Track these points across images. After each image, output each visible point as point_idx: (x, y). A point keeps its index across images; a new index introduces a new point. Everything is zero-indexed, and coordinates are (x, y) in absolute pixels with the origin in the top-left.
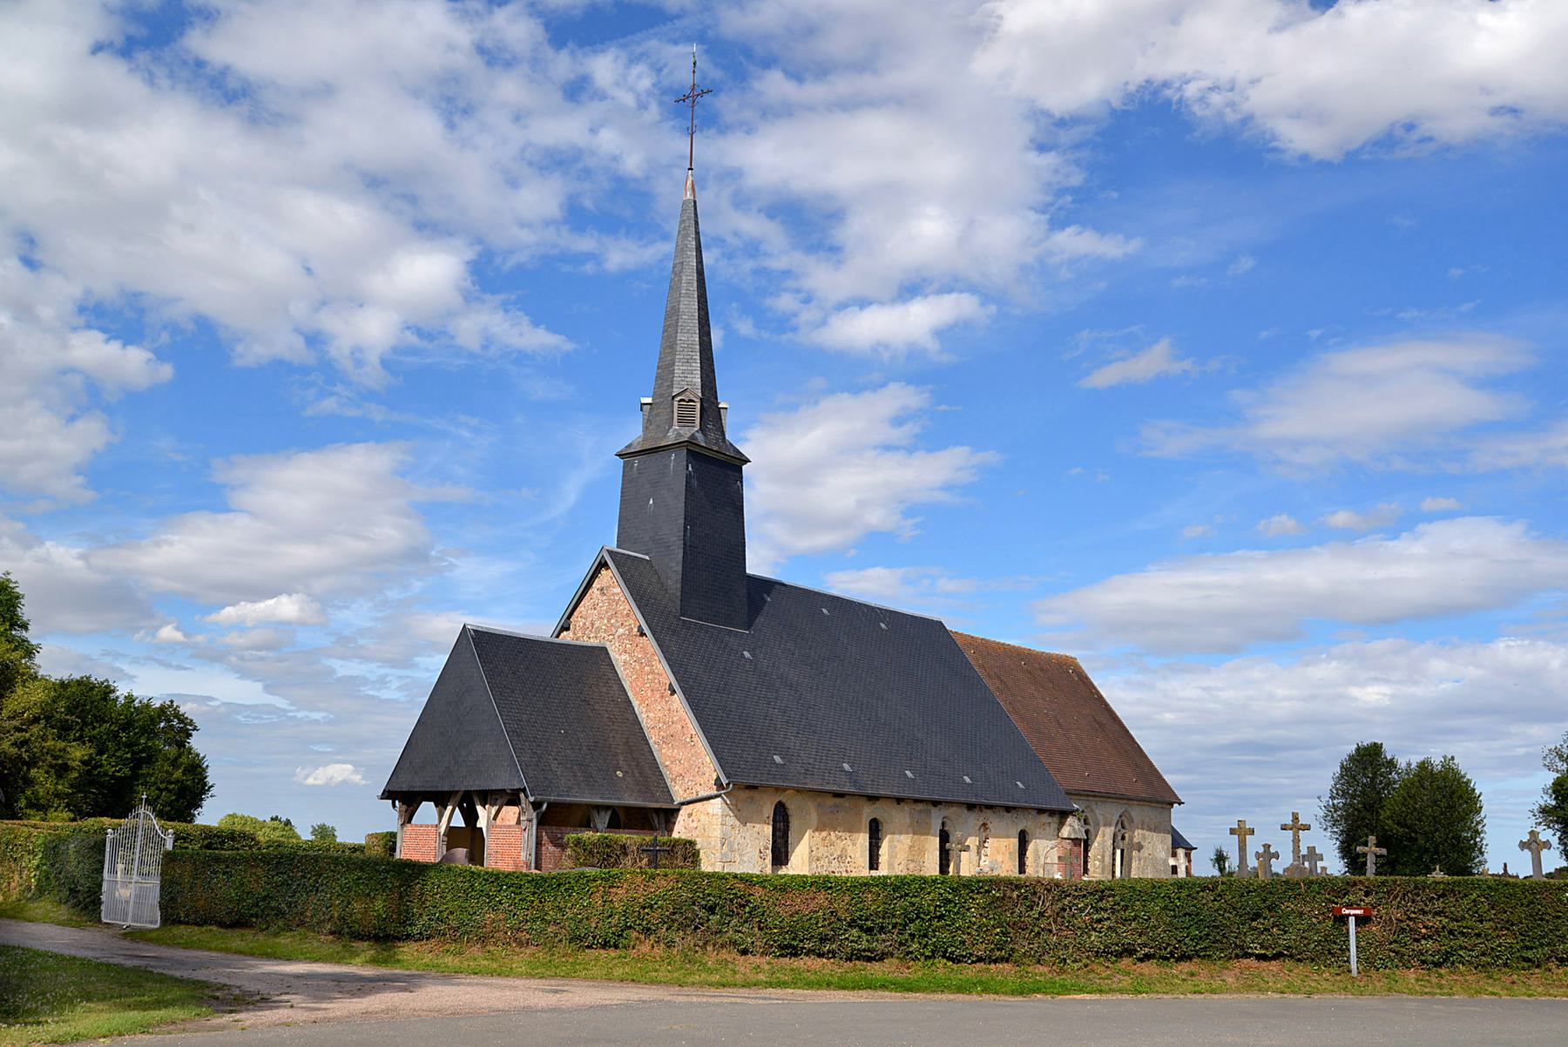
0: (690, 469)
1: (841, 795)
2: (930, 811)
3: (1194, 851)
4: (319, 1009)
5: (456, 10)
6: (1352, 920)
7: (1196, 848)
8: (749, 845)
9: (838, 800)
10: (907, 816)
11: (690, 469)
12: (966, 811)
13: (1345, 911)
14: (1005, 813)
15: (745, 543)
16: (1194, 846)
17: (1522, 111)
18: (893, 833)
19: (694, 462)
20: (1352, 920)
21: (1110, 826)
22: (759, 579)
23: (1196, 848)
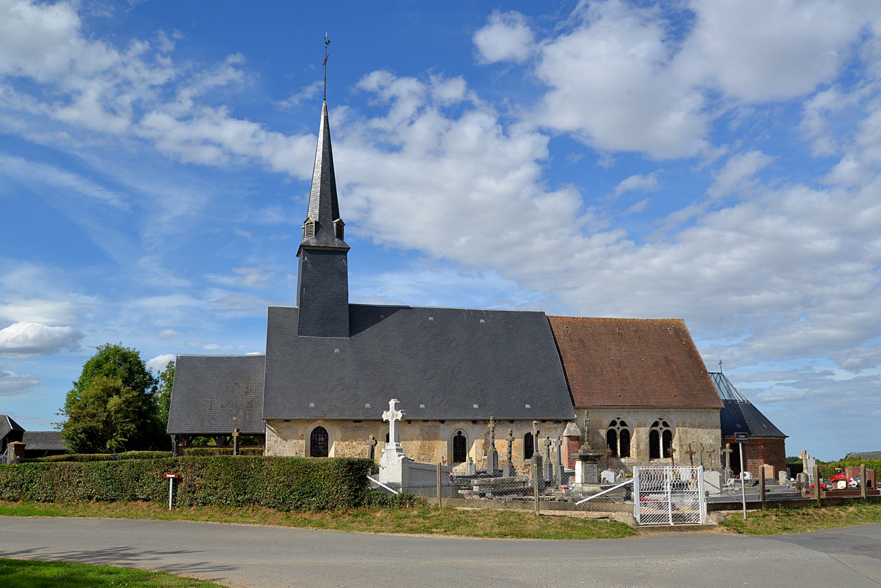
0: (306, 259)
1: (359, 421)
2: (439, 426)
3: (786, 438)
4: (202, 568)
5: (648, 20)
6: (171, 480)
7: (788, 437)
8: (288, 450)
9: (358, 424)
10: (418, 429)
11: (306, 259)
12: (471, 424)
13: (168, 476)
14: (509, 424)
15: (348, 291)
16: (787, 435)
17: (375, 146)
18: (406, 440)
19: (308, 254)
20: (171, 480)
21: (645, 426)
22: (390, 307)
23: (788, 437)
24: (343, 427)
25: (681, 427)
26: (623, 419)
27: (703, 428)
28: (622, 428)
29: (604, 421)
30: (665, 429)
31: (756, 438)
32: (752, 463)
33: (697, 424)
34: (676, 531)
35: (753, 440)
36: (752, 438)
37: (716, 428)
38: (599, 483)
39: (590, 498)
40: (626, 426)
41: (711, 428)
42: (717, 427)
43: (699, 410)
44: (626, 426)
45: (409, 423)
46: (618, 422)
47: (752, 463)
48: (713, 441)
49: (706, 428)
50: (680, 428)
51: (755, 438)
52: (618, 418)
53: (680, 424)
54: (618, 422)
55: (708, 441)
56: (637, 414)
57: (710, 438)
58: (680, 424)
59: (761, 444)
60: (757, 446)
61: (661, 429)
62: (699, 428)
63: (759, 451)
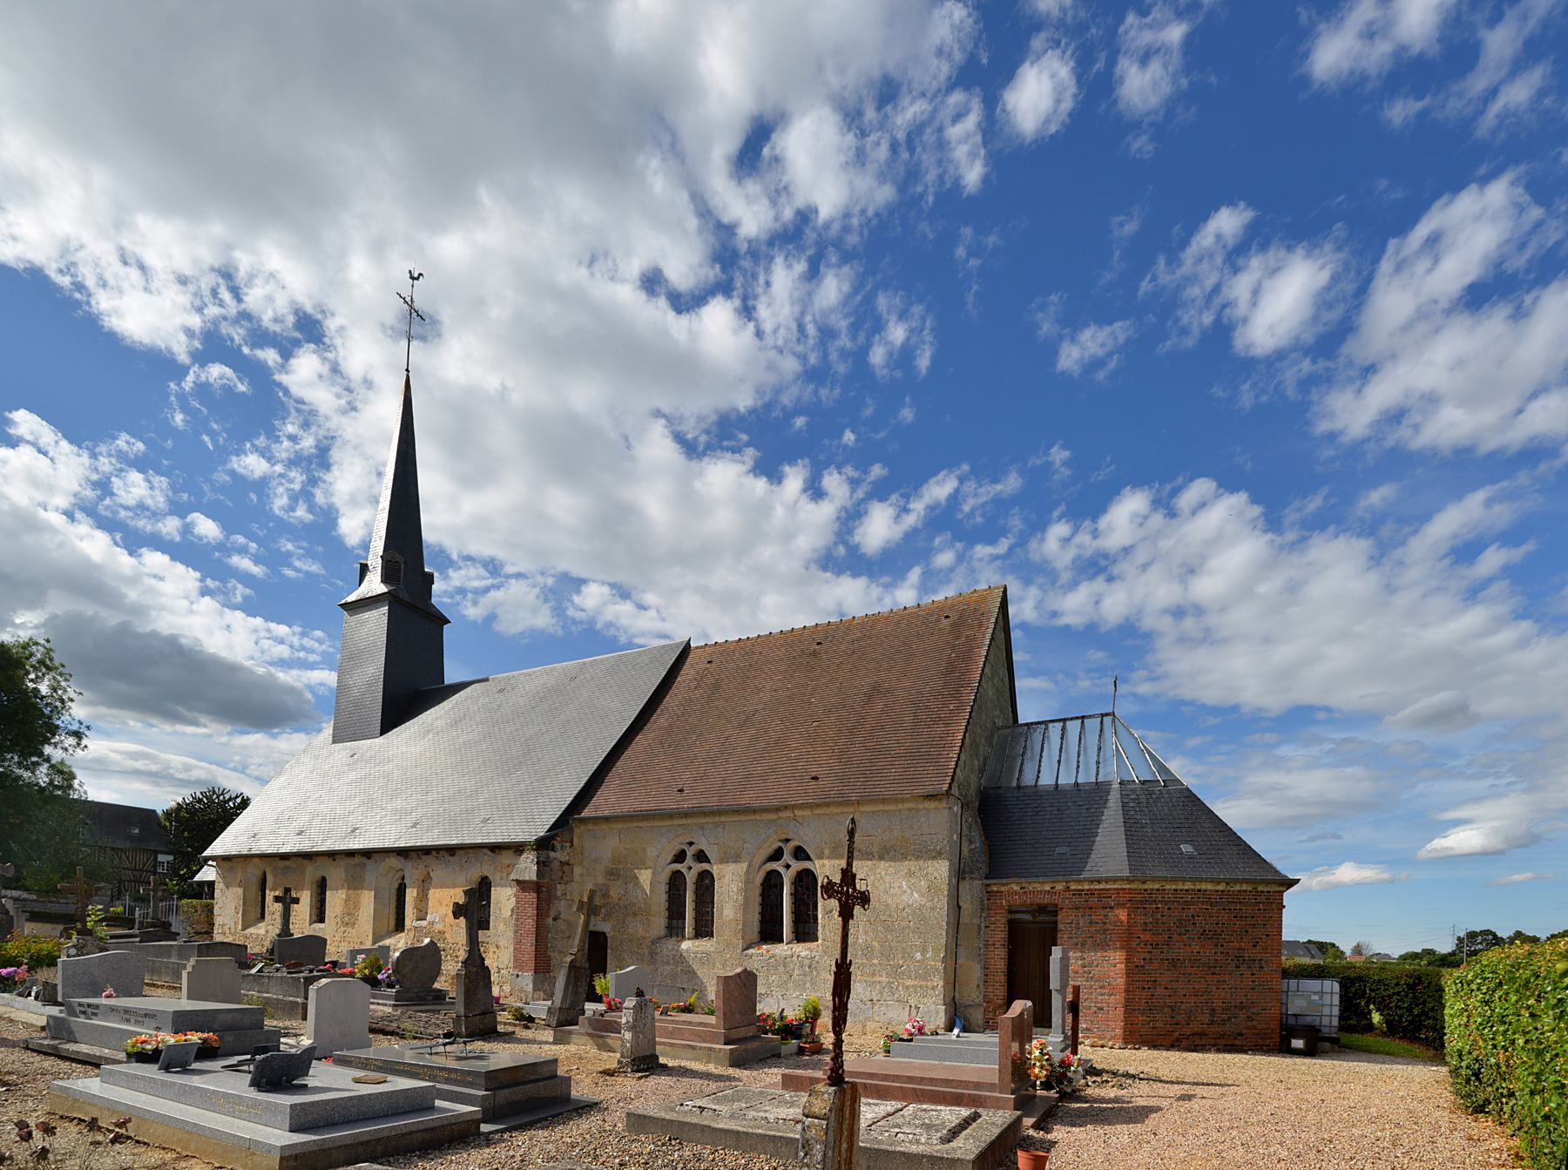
2: (365, 865)
24: (1399, 268)
25: (829, 858)
26: (702, 844)
27: (893, 859)
28: (797, 866)
29: (648, 850)
30: (797, 866)
31: (1102, 886)
32: (1080, 962)
33: (875, 849)
34: (488, 1140)
35: (1091, 892)
36: (1086, 887)
37: (934, 858)
38: (806, 1111)
39: (349, 1053)
40: (808, 858)
41: (918, 858)
42: (938, 855)
43: (880, 807)
44: (808, 858)
45: (451, 855)
46: (788, 850)
47: (1080, 962)
48: (922, 895)
49: (904, 857)
50: (826, 862)
51: (1097, 887)
52: (691, 844)
53: (827, 852)
54: (690, 852)
55: (904, 897)
56: (720, 829)
57: (912, 887)
58: (827, 852)
59: (1122, 906)
60: (1102, 912)
61: (788, 866)
62: (881, 858)
63: (1108, 926)
